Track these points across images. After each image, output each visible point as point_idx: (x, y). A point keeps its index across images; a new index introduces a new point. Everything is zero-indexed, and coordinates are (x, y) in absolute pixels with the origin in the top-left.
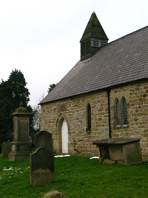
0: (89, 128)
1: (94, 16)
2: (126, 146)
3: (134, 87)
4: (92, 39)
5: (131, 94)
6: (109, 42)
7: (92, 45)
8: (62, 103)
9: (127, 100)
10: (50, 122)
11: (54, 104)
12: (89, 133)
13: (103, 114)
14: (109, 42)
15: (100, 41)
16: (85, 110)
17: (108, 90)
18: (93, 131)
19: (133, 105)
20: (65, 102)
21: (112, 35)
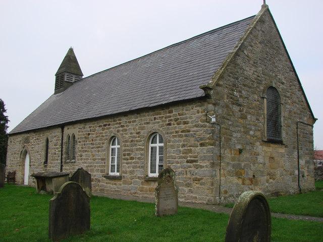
0: (46, 162)
1: (71, 50)
2: (55, 179)
3: (82, 126)
4: (66, 74)
5: (79, 132)
6: (83, 77)
7: (66, 80)
8: (26, 136)
9: (77, 137)
10: (15, 153)
11: (20, 136)
12: (46, 166)
13: (57, 148)
14: (83, 77)
15: (74, 76)
16: (45, 144)
17: (62, 126)
18: (49, 164)
19: (80, 142)
20: (29, 135)
21: (87, 70)
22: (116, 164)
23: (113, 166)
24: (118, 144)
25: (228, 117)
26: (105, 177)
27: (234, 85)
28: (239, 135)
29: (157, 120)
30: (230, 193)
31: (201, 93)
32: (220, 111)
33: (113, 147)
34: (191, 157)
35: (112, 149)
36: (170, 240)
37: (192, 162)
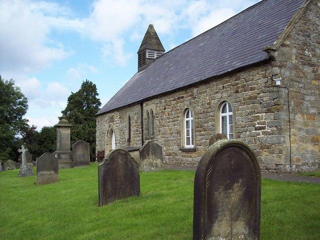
1: (151, 27)
4: (147, 51)
7: (147, 57)
15: (156, 52)
17: (141, 103)
20: (113, 114)
22: (190, 136)
23: (188, 139)
24: (230, 111)
25: (298, 79)
26: (181, 150)
27: (305, 44)
28: (313, 98)
29: (225, 89)
30: (304, 161)
31: (264, 56)
32: (287, 73)
33: (224, 114)
34: (258, 124)
35: (223, 118)
36: (160, 238)
37: (260, 129)
